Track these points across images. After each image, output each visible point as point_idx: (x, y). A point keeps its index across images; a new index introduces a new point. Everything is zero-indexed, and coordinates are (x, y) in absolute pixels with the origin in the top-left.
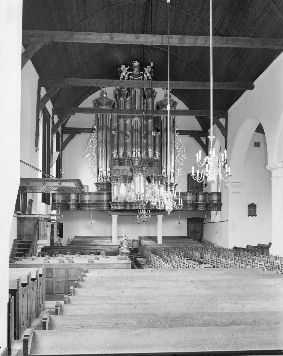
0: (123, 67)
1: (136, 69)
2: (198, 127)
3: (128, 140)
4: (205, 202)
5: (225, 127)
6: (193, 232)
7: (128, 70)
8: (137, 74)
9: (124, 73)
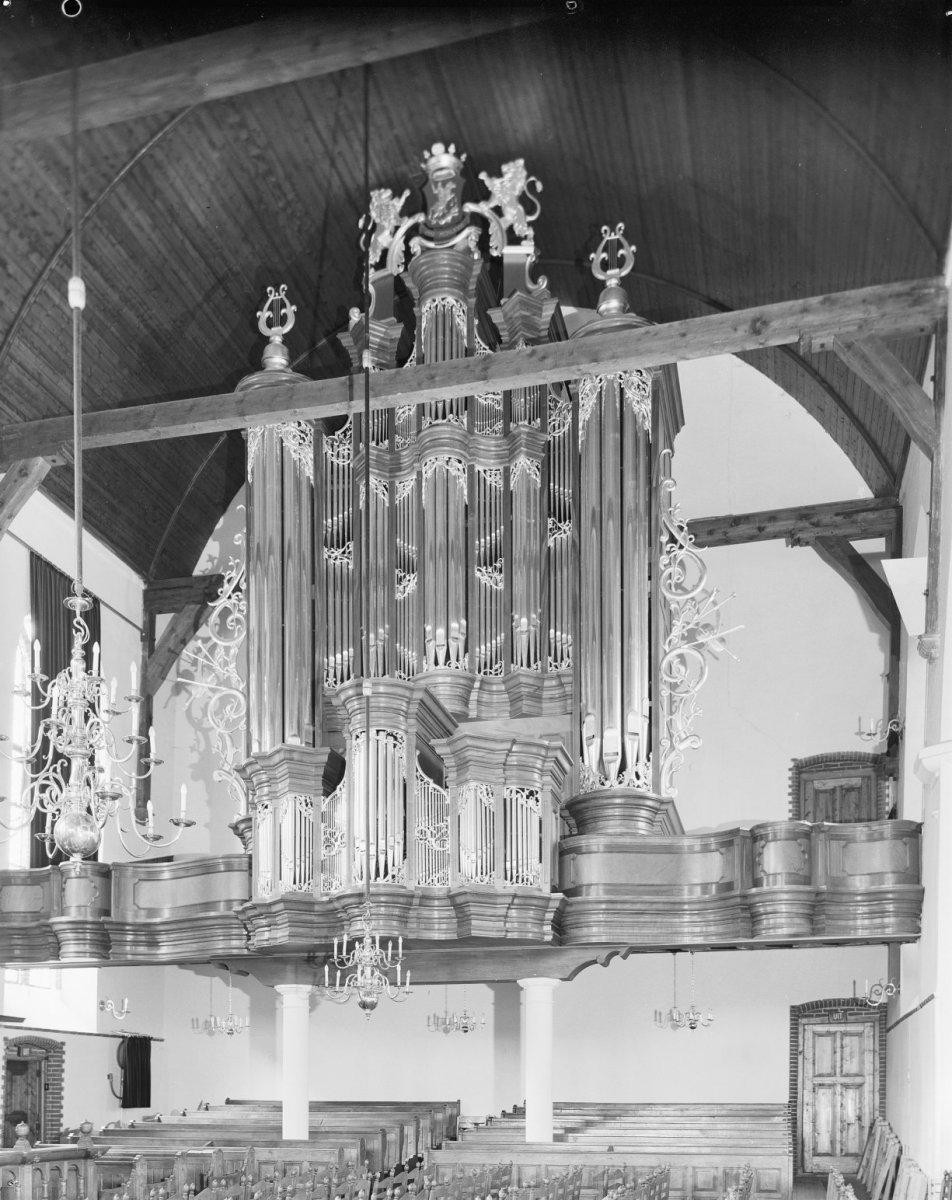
0: (381, 197)
1: (445, 194)
2: (840, 479)
3: (407, 589)
4: (809, 884)
5: (932, 398)
6: (858, 1080)
7: (407, 211)
8: (449, 219)
9: (387, 233)
